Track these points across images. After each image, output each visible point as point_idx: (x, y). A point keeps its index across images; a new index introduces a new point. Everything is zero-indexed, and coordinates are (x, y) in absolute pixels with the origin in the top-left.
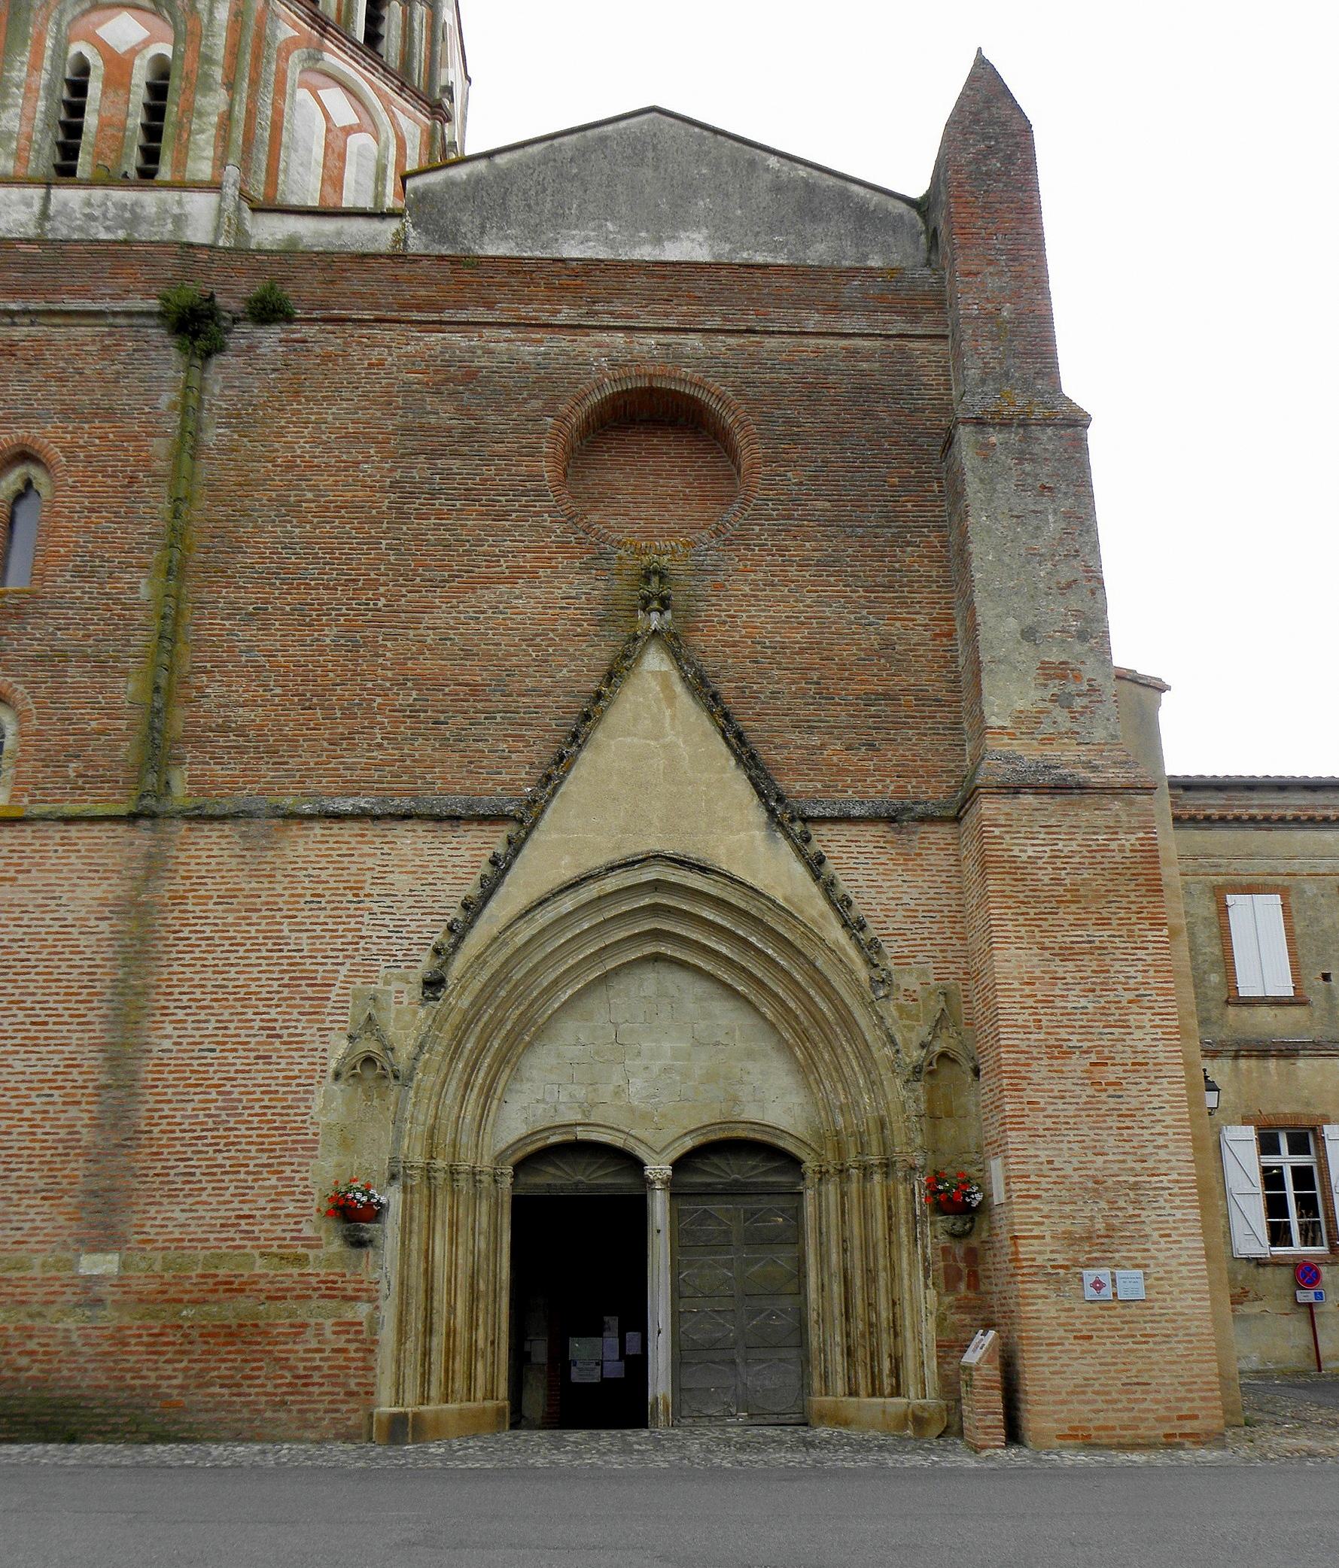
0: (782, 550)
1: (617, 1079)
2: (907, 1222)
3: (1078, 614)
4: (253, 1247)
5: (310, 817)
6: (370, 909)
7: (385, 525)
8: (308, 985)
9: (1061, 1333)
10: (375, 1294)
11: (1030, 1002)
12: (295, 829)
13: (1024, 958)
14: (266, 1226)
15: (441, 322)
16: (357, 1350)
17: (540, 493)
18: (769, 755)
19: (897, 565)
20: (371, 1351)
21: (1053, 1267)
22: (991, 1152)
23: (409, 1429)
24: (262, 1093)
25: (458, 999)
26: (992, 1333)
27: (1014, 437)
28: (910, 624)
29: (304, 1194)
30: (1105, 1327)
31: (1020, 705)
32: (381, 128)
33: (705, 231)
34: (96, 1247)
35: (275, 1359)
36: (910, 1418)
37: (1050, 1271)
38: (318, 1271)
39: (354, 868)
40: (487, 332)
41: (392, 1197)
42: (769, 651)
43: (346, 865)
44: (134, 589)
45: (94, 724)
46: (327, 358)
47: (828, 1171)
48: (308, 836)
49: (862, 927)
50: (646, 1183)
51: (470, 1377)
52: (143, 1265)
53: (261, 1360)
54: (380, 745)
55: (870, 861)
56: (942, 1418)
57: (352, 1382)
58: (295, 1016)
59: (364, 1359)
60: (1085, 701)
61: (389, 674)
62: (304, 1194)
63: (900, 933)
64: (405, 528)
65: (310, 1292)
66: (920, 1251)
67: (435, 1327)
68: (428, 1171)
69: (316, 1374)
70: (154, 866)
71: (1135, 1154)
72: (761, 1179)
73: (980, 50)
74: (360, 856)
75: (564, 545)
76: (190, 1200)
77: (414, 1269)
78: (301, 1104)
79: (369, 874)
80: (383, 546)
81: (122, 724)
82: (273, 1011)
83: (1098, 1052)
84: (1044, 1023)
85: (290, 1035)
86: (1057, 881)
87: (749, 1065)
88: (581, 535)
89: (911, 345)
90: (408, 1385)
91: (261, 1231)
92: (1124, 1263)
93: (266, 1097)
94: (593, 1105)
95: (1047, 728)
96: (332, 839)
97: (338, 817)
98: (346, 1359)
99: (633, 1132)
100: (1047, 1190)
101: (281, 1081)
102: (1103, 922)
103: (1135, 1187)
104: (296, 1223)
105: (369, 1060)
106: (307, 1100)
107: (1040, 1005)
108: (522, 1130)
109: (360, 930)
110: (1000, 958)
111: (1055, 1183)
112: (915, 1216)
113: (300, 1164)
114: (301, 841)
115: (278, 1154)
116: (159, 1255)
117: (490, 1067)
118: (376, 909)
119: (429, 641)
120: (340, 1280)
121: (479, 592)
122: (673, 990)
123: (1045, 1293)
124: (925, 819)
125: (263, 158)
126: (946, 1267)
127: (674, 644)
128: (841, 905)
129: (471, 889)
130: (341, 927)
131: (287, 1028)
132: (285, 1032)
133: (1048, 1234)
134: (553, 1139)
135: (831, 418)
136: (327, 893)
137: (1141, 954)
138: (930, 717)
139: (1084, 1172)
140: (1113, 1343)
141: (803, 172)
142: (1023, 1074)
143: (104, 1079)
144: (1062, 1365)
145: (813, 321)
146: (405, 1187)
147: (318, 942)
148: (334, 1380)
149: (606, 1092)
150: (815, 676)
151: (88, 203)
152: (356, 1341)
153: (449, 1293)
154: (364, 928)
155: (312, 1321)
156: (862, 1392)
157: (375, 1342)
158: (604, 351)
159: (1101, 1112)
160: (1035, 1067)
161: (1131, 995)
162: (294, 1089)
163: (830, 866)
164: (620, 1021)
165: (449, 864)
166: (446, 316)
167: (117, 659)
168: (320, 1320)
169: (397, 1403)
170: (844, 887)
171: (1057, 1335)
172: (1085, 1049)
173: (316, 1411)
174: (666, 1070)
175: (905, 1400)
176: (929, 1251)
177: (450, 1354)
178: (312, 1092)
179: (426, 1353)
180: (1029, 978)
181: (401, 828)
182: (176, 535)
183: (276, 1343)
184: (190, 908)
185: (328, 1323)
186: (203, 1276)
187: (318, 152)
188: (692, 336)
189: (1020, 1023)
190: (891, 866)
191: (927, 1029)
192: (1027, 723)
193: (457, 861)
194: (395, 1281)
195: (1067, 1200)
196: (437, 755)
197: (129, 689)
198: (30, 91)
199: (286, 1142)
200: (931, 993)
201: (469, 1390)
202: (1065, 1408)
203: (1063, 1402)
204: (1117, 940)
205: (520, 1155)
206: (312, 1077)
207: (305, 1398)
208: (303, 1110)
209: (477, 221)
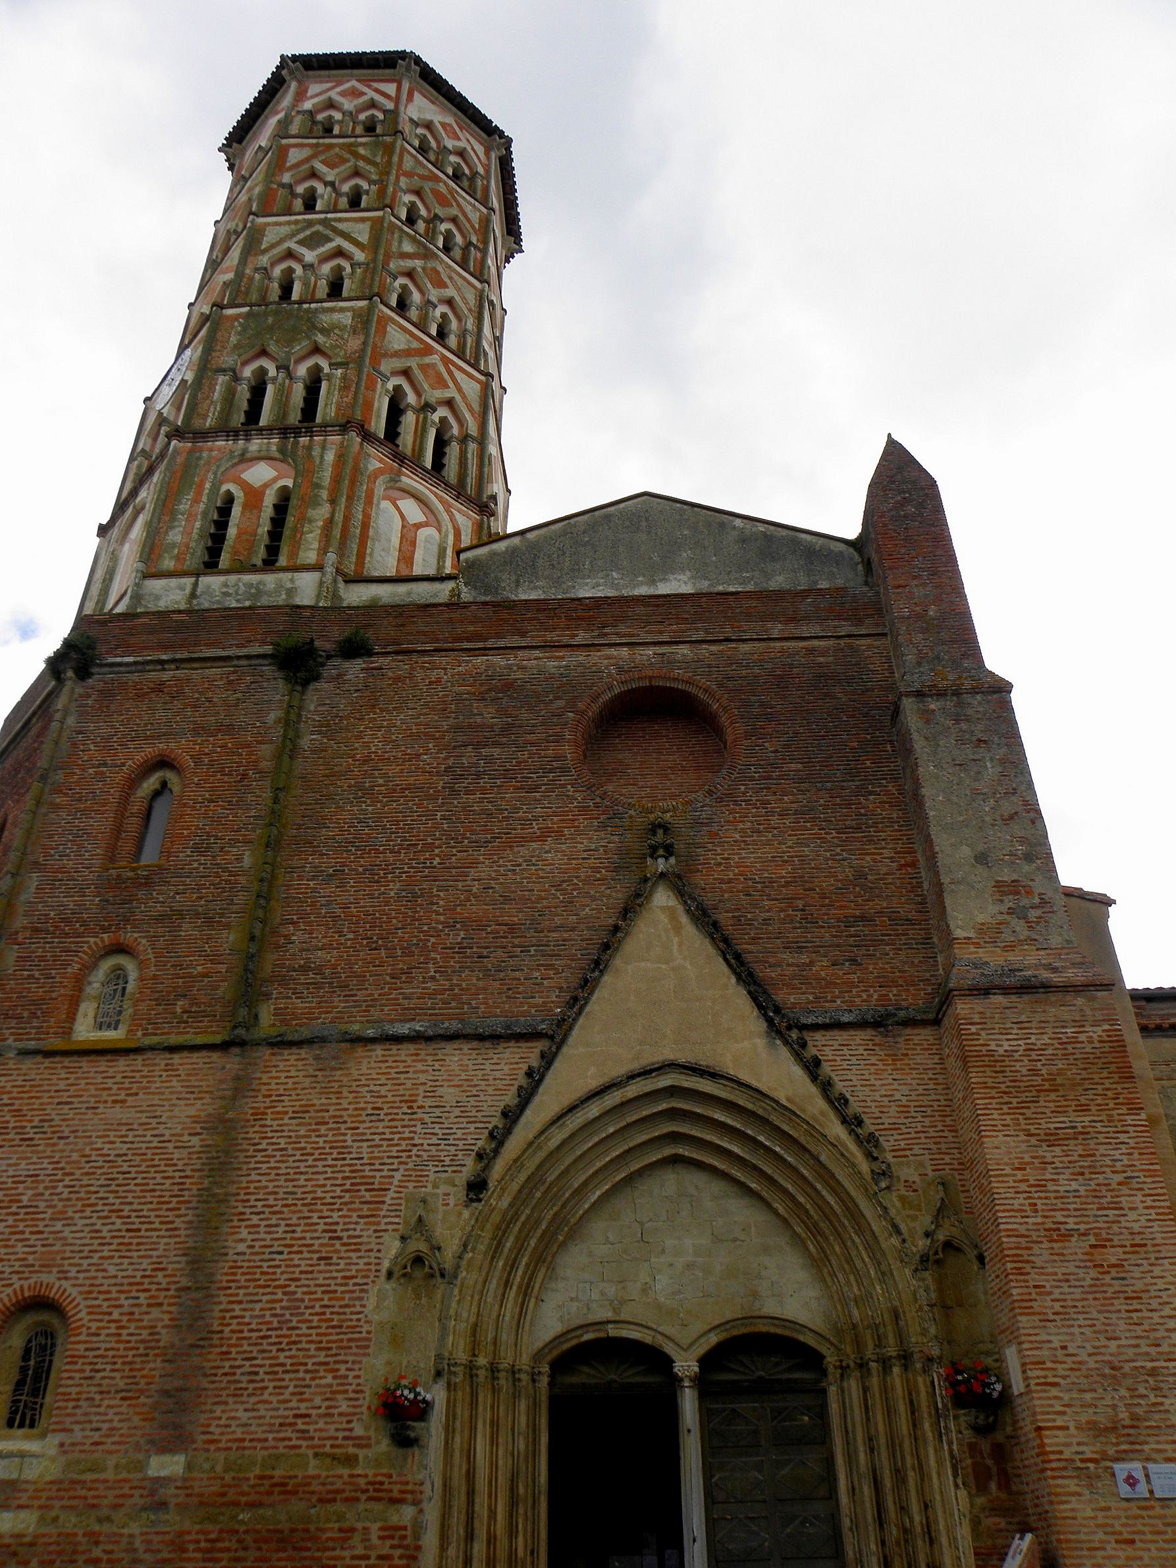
2: (930, 1415)
3: (1023, 841)
5: (373, 1040)
6: (421, 1119)
8: (366, 1190)
9: (1101, 1536)
11: (1023, 1187)
12: (360, 1051)
13: (1013, 1144)
14: (321, 1425)
15: (485, 649)
17: (564, 770)
18: (764, 972)
19: (863, 811)
21: (1082, 1461)
25: (499, 1201)
27: (950, 703)
28: (878, 857)
30: (1146, 1529)
31: (981, 918)
32: (443, 524)
33: (688, 573)
34: (165, 1448)
37: (1079, 1464)
39: (409, 1084)
40: (520, 653)
41: (437, 1395)
42: (759, 886)
44: (239, 859)
45: (199, 968)
46: (398, 679)
50: (674, 1381)
52: (206, 1466)
54: (433, 978)
58: (354, 1219)
60: (1039, 912)
61: (442, 918)
62: (357, 1392)
63: (895, 1127)
65: (359, 1494)
66: (946, 1447)
67: (477, 1532)
68: (471, 1368)
70: (241, 1086)
71: (1148, 1337)
72: (785, 1376)
73: (889, 435)
75: (584, 809)
76: (253, 1399)
79: (422, 1088)
81: (223, 968)
82: (335, 1215)
83: (1096, 1235)
84: (1039, 1207)
85: (349, 1237)
86: (1034, 1072)
88: (598, 800)
92: (1154, 1456)
93: (326, 1297)
94: (622, 1303)
95: (1007, 936)
97: (397, 1039)
99: (660, 1329)
100: (1064, 1377)
102: (1083, 1109)
103: (1153, 1372)
106: (361, 1299)
107: (1034, 1189)
109: (412, 1138)
112: (937, 1409)
114: (365, 1061)
116: (221, 1456)
117: (528, 1266)
118: (427, 1120)
119: (475, 890)
121: (516, 849)
123: (1078, 1489)
125: (355, 547)
127: (679, 884)
128: (838, 1103)
129: (510, 1098)
130: (397, 1136)
132: (345, 1234)
133: (1072, 1425)
135: (798, 700)
136: (385, 1106)
137: (1123, 1137)
139: (1099, 1358)
140: (1159, 1549)
141: (761, 528)
142: (1026, 1258)
143: (185, 1282)
145: (777, 630)
146: (449, 1384)
150: (800, 903)
151: (226, 585)
153: (490, 1497)
155: (359, 1525)
157: (418, 1548)
158: (614, 661)
159: (1108, 1295)
161: (1119, 1178)
163: (826, 1068)
164: (645, 1220)
165: (491, 1078)
166: (489, 644)
167: (222, 915)
168: (368, 1524)
170: (840, 1087)
171: (1096, 1538)
172: (1082, 1231)
174: (690, 1266)
178: (366, 1291)
180: (1020, 1163)
181: (449, 1047)
182: (275, 817)
184: (269, 1122)
185: (375, 1527)
186: (261, 1477)
187: (396, 541)
189: (1016, 1207)
190: (881, 1067)
191: (929, 1219)
192: (989, 934)
193: (498, 1074)
195: (1086, 1387)
196: (481, 984)
197: (230, 938)
198: (191, 517)
199: (341, 1341)
204: (1098, 1124)
208: (358, 1309)
209: (514, 578)
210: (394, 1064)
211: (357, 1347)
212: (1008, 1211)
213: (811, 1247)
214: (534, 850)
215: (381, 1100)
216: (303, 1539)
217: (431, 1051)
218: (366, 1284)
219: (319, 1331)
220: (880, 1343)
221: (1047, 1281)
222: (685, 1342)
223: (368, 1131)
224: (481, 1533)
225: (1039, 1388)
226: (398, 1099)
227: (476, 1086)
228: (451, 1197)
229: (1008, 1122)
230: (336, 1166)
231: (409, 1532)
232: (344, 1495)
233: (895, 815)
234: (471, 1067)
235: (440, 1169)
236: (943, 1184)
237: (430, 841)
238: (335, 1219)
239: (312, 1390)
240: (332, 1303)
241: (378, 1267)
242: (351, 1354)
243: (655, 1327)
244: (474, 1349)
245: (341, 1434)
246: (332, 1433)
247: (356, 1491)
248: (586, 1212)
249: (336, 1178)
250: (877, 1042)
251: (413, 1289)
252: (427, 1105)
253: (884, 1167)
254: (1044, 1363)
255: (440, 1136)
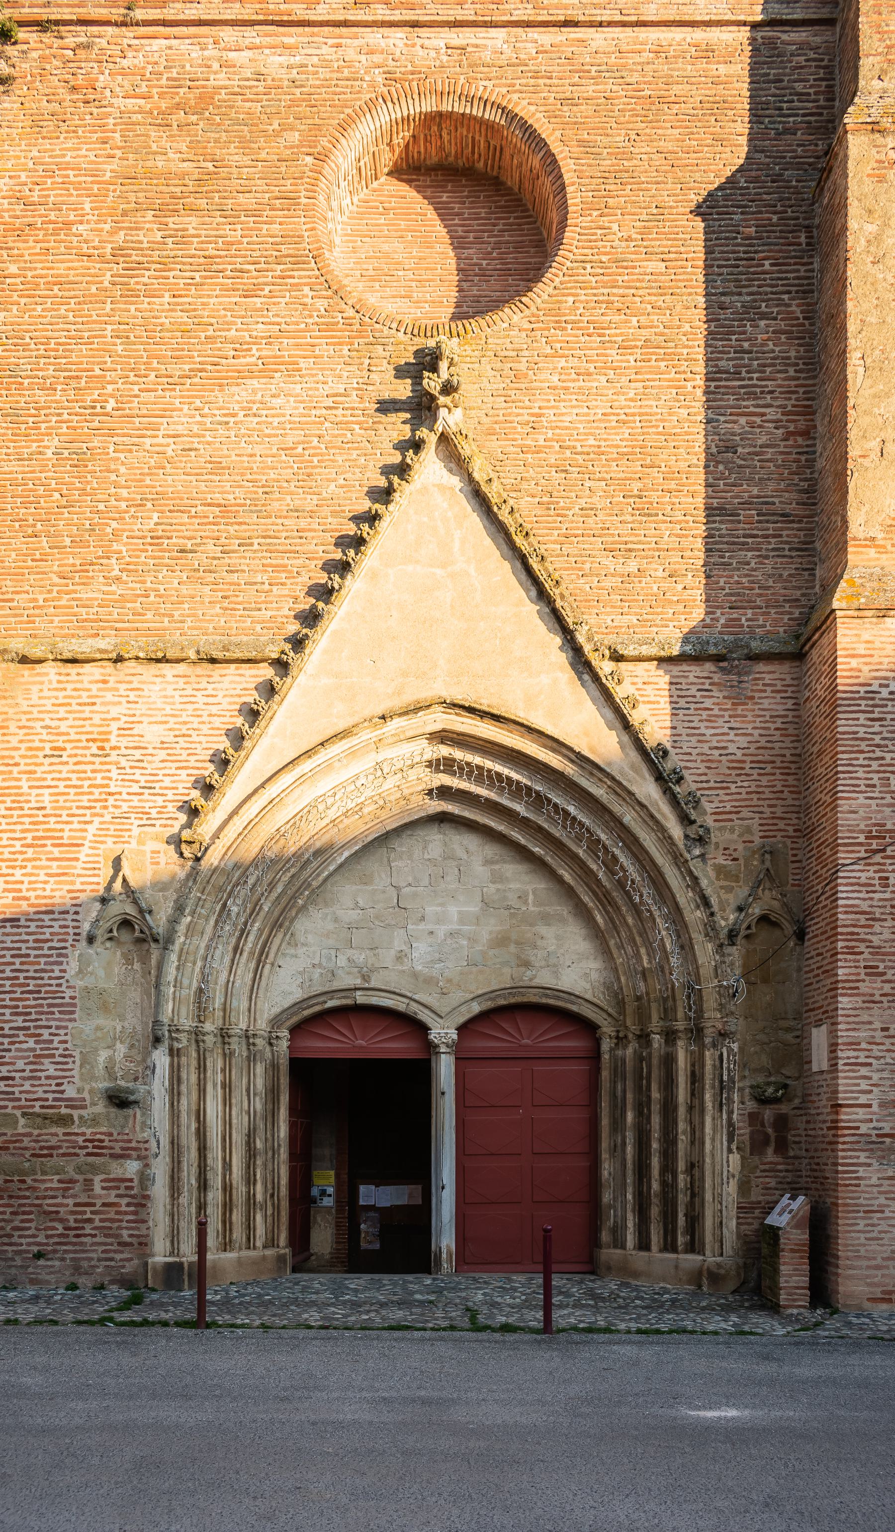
0: (600, 329)
1: (399, 943)
2: (713, 1087)
4: (14, 1107)
6: (117, 763)
7: (109, 306)
8: (53, 845)
9: (882, 1201)
10: (144, 1153)
13: (874, 807)
14: (27, 1086)
15: (165, 23)
16: (128, 1205)
19: (746, 345)
20: (144, 1206)
22: (812, 1019)
23: (186, 1278)
24: (13, 956)
26: (801, 1198)
28: (758, 420)
29: (65, 1056)
35: (45, 1212)
36: (705, 1273)
38: (83, 1129)
39: (97, 719)
43: (87, 715)
47: (626, 1037)
48: (42, 683)
49: (680, 780)
50: (431, 1048)
51: (249, 1227)
53: (30, 1213)
55: (692, 706)
56: (739, 1274)
57: (125, 1233)
58: (42, 878)
59: (135, 1213)
62: (65, 1056)
64: (133, 307)
65: (77, 1151)
66: (725, 1116)
67: (210, 1182)
68: (197, 1035)
69: (88, 1226)
74: (103, 704)
77: (184, 1129)
78: (55, 967)
80: (109, 333)
87: (543, 930)
89: (785, 37)
90: (183, 1235)
91: (21, 1092)
93: (18, 961)
96: (70, 686)
98: (117, 1213)
99: (416, 997)
101: (31, 944)
104: (58, 1085)
105: (126, 923)
106: (61, 963)
108: (298, 995)
109: (107, 786)
110: (846, 808)
111: (888, 1051)
112: (721, 1081)
113: (58, 1028)
114: (35, 688)
115: (33, 1017)
117: (261, 931)
119: (170, 453)
120: (107, 1138)
122: (460, 853)
123: (868, 1161)
124: (755, 658)
126: (752, 1134)
130: (86, 783)
131: (35, 890)
132: (32, 894)
134: (330, 1004)
136: (68, 746)
138: (774, 536)
142: (862, 936)
144: (880, 1232)
146: (171, 1050)
147: (61, 798)
148: (106, 1232)
149: (387, 958)
150: (636, 486)
152: (126, 1196)
153: (224, 1150)
154: (112, 783)
156: (654, 1247)
157: (147, 1197)
158: (377, 58)
160: (877, 928)
162: (46, 952)
164: (402, 884)
165: (205, 713)
168: (90, 1176)
169: (172, 1254)
171: (876, 1202)
173: (91, 1259)
175: (701, 1258)
176: (735, 1116)
177: (227, 1206)
178: (66, 956)
179: (202, 1207)
183: (45, 1197)
188: (493, 32)
189: (863, 880)
190: (716, 712)
191: (746, 891)
193: (214, 709)
194: (165, 1141)
199: (42, 1006)
200: (754, 853)
201: (249, 1239)
202: (879, 1273)
203: (878, 1267)
205: (295, 1019)
206: (66, 941)
207: (77, 1248)
208: (57, 974)
210: (75, 693)
211: (60, 1012)
212: (852, 884)
213: (599, 919)
214: (254, 391)
215: (62, 738)
216: (19, 1189)
217: (122, 677)
218: (65, 948)
219: (13, 996)
220: (668, 1013)
221: (883, 961)
222: (443, 1011)
223: (49, 776)
224: (216, 1181)
225: (847, 1068)
226: (84, 737)
227: (185, 723)
228: (162, 855)
229: (875, 781)
230: (12, 816)
231: (136, 1183)
232: (61, 1151)
233: (793, 354)
234: (178, 699)
235: (144, 822)
236: (771, 852)
237: (98, 372)
238: (18, 877)
239: (12, 1054)
240: (25, 967)
241: (77, 931)
242: (55, 1020)
243: (409, 995)
244: (201, 1011)
245: (51, 1096)
246: (40, 1095)
247: (74, 1148)
248: (331, 875)
249: (14, 831)
250: (716, 680)
251: (122, 953)
252: (122, 745)
253: (701, 831)
254: (859, 1044)
255: (143, 784)
